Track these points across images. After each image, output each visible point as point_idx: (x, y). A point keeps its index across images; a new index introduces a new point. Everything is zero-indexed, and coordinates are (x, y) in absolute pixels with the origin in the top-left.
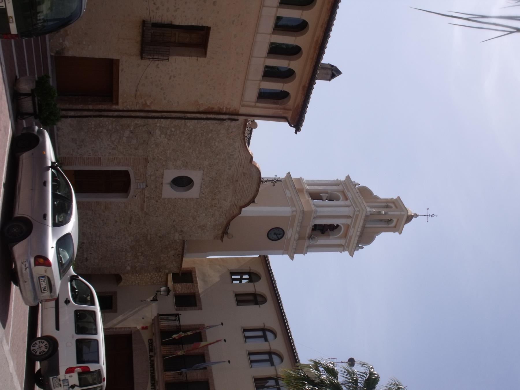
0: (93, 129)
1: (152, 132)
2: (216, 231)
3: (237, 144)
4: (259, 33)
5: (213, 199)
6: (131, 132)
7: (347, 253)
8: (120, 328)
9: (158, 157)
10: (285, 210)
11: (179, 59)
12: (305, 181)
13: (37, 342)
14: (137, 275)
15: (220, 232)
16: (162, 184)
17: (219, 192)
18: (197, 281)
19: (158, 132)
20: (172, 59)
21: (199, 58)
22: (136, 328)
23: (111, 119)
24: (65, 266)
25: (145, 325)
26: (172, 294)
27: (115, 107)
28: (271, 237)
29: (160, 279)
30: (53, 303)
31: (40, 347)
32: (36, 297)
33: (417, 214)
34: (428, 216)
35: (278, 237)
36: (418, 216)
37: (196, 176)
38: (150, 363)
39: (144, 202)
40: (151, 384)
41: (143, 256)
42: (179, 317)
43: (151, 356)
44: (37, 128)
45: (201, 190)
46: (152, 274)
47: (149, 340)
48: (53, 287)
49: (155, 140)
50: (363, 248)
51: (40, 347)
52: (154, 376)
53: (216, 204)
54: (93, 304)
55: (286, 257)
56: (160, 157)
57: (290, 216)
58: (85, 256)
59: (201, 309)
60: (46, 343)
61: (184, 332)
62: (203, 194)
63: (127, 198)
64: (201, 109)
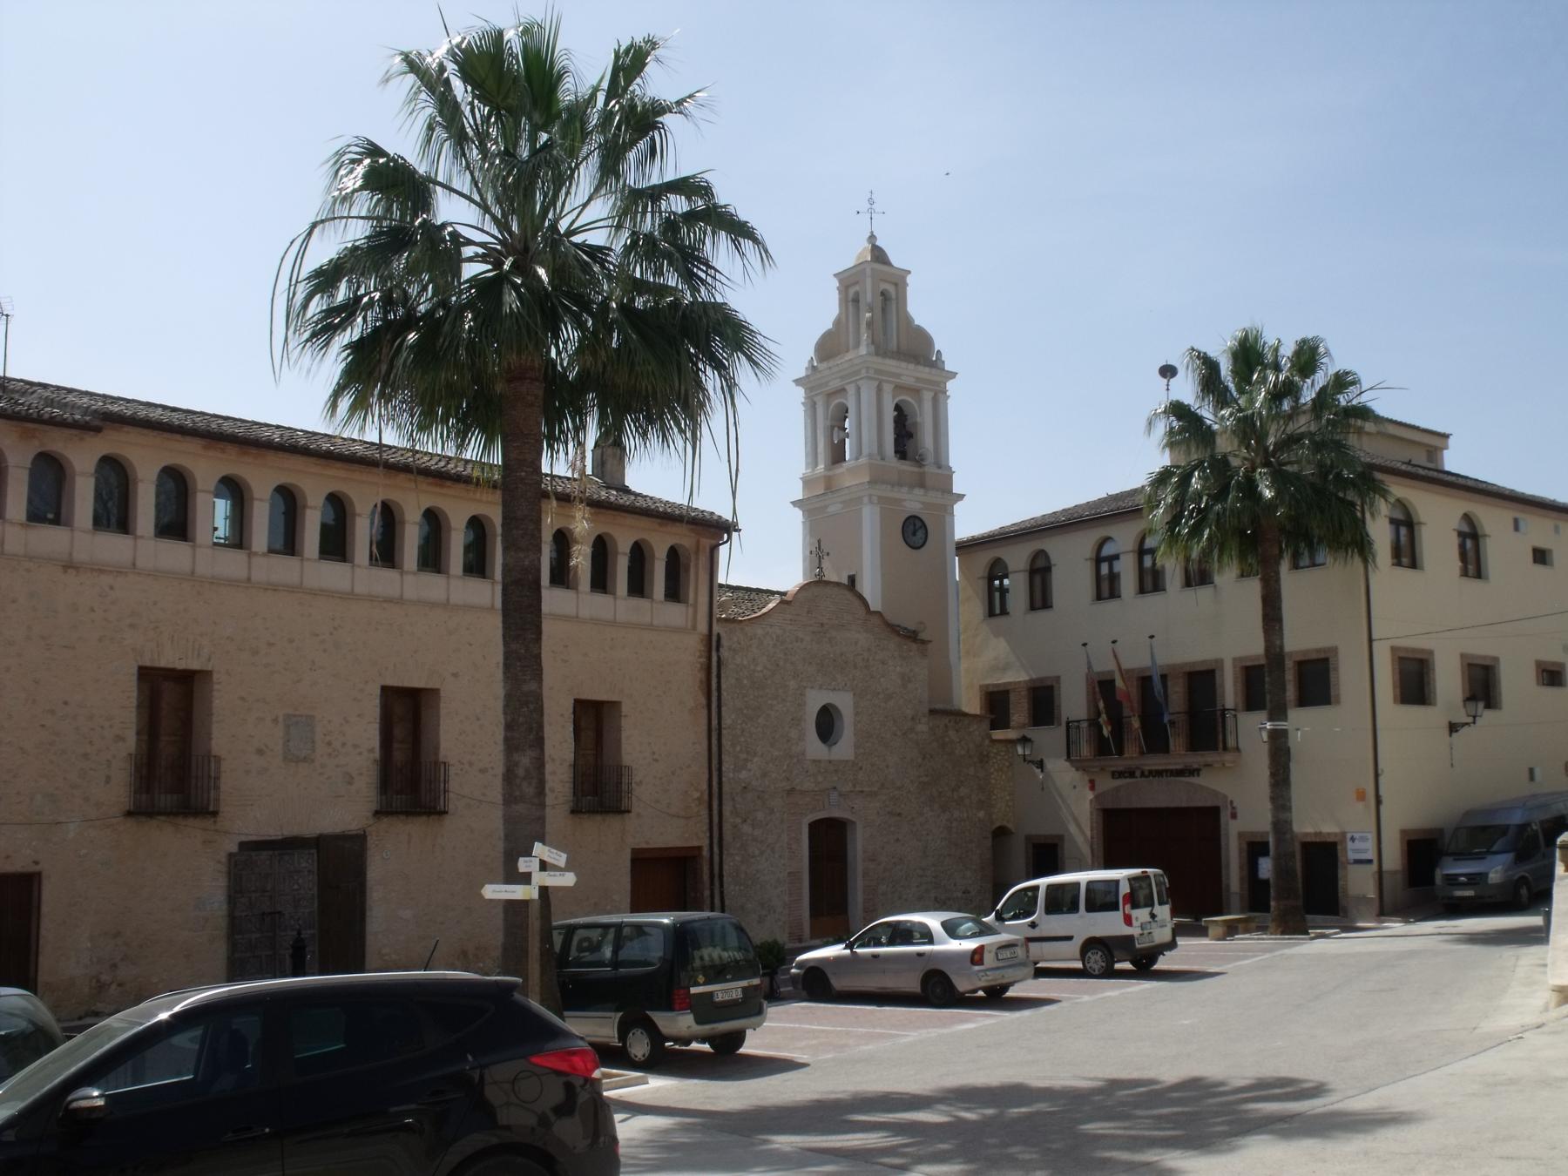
0: (742, 888)
1: (743, 785)
2: (911, 654)
3: (760, 632)
4: (577, 614)
5: (855, 667)
6: (745, 821)
7: (950, 385)
8: (1091, 830)
9: (784, 771)
10: (869, 518)
11: (626, 747)
12: (808, 471)
13: (1088, 966)
14: (994, 797)
15: (914, 646)
16: (830, 762)
17: (842, 655)
18: (1005, 684)
19: (743, 775)
20: (626, 759)
21: (623, 714)
22: (1091, 801)
23: (724, 857)
24: (983, 929)
25: (1088, 785)
26: (1031, 733)
27: (705, 853)
28: (921, 542)
29: (1003, 754)
30: (1032, 946)
31: (1096, 962)
32: (1023, 964)
33: (867, 237)
34: (871, 211)
35: (921, 527)
36: (872, 232)
37: (815, 701)
38: (1154, 777)
39: (862, 792)
40: (1189, 776)
41: (959, 787)
42: (1072, 722)
43: (1143, 775)
44: (793, 971)
45: (839, 689)
46: (992, 770)
47: (1113, 777)
48: (1011, 943)
49: (757, 779)
50: (938, 351)
51: (1096, 962)
52: (1177, 770)
53: (863, 659)
54: (1036, 888)
55: (958, 508)
56: (785, 767)
57: (881, 508)
58: (959, 894)
59: (1058, 679)
60: (1089, 954)
61: (1099, 714)
62: (846, 685)
63: (854, 823)
64: (703, 701)
